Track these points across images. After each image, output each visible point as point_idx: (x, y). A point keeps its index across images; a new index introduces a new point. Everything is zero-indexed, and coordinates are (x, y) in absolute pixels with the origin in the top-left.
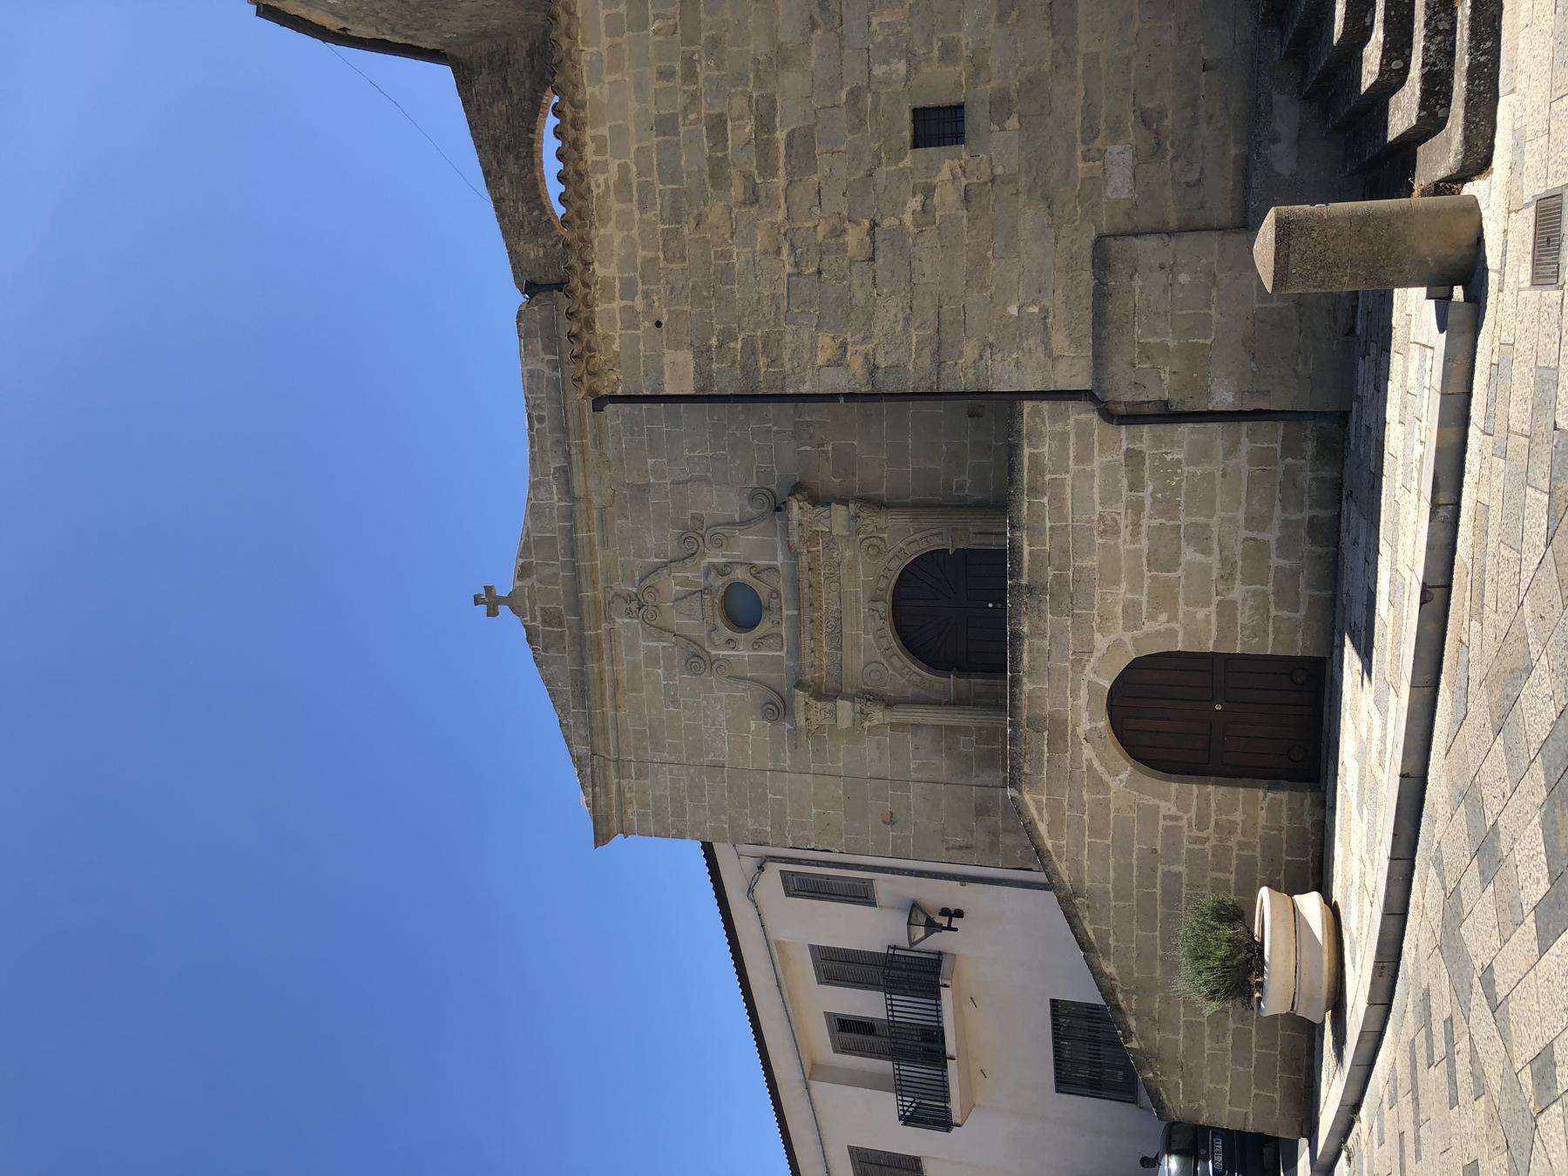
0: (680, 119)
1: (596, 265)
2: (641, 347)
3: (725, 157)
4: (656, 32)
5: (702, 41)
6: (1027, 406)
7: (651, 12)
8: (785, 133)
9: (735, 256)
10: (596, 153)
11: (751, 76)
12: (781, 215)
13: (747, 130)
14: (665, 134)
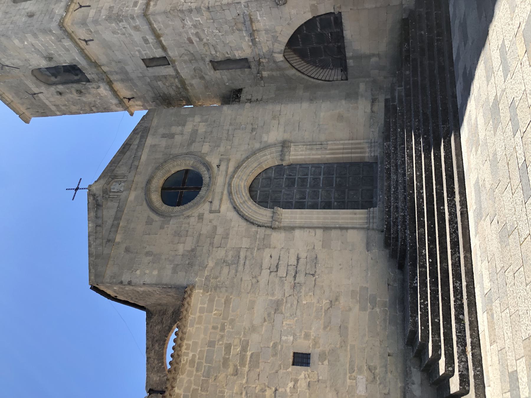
0: (216, 343)
1: (176, 388)
3: (229, 358)
4: (215, 314)
5: (229, 319)
7: (214, 308)
8: (250, 353)
9: (226, 393)
10: (186, 349)
11: (242, 333)
12: (244, 381)
13: (238, 350)
14: (210, 347)
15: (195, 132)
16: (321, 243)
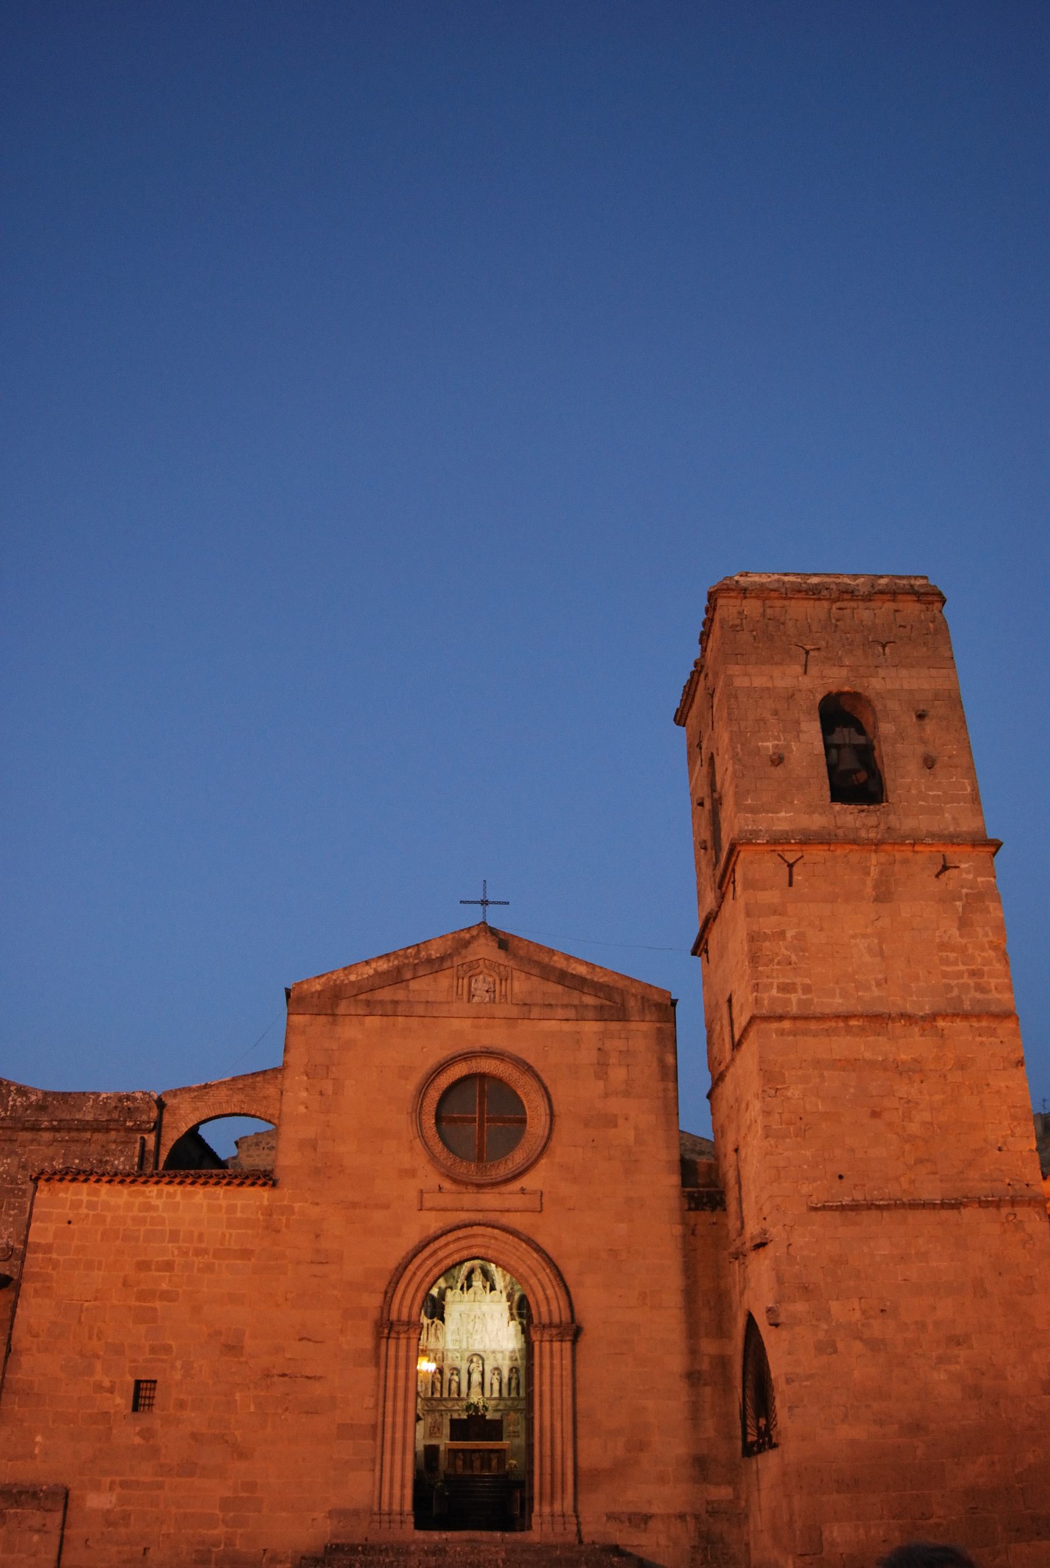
2: (59, 1210)
6: (416, 1450)
7: (234, 1232)
15: (611, 1121)
16: (348, 1422)
